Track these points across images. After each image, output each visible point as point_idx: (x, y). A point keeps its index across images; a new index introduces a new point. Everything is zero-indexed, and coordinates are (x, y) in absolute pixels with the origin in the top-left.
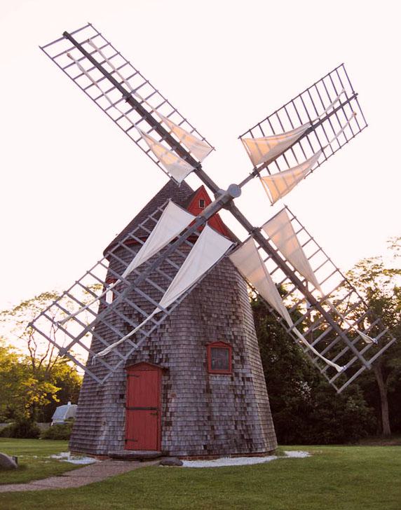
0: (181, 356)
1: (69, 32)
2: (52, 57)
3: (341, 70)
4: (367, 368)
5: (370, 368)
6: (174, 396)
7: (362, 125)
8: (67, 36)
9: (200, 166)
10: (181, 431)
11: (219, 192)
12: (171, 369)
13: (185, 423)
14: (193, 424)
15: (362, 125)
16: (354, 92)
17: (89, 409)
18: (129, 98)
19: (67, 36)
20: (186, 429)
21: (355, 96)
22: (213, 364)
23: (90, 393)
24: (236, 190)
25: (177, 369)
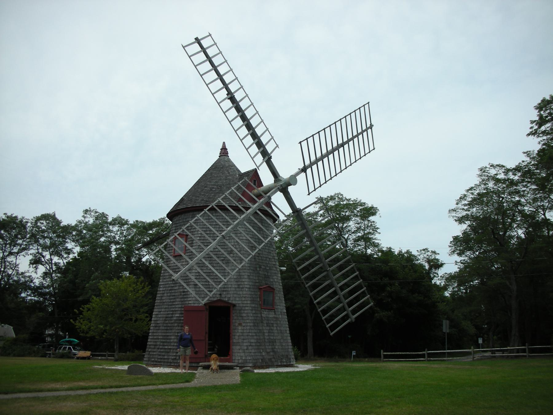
0: (244, 296)
1: (199, 38)
2: (190, 55)
3: (367, 106)
4: (351, 321)
5: (354, 320)
6: (240, 324)
7: (371, 148)
8: (198, 41)
9: (271, 158)
10: (247, 349)
11: (280, 178)
12: (237, 305)
13: (249, 344)
14: (254, 345)
15: (371, 148)
16: (371, 124)
17: (154, 336)
18: (231, 97)
19: (198, 41)
20: (250, 348)
21: (371, 126)
22: (403, 268)
23: (345, 276)
24: (292, 181)
25: (241, 305)
